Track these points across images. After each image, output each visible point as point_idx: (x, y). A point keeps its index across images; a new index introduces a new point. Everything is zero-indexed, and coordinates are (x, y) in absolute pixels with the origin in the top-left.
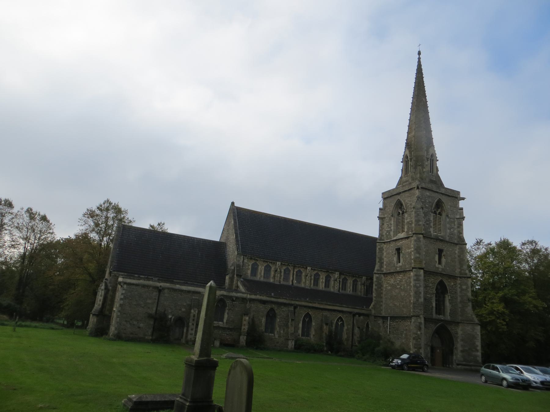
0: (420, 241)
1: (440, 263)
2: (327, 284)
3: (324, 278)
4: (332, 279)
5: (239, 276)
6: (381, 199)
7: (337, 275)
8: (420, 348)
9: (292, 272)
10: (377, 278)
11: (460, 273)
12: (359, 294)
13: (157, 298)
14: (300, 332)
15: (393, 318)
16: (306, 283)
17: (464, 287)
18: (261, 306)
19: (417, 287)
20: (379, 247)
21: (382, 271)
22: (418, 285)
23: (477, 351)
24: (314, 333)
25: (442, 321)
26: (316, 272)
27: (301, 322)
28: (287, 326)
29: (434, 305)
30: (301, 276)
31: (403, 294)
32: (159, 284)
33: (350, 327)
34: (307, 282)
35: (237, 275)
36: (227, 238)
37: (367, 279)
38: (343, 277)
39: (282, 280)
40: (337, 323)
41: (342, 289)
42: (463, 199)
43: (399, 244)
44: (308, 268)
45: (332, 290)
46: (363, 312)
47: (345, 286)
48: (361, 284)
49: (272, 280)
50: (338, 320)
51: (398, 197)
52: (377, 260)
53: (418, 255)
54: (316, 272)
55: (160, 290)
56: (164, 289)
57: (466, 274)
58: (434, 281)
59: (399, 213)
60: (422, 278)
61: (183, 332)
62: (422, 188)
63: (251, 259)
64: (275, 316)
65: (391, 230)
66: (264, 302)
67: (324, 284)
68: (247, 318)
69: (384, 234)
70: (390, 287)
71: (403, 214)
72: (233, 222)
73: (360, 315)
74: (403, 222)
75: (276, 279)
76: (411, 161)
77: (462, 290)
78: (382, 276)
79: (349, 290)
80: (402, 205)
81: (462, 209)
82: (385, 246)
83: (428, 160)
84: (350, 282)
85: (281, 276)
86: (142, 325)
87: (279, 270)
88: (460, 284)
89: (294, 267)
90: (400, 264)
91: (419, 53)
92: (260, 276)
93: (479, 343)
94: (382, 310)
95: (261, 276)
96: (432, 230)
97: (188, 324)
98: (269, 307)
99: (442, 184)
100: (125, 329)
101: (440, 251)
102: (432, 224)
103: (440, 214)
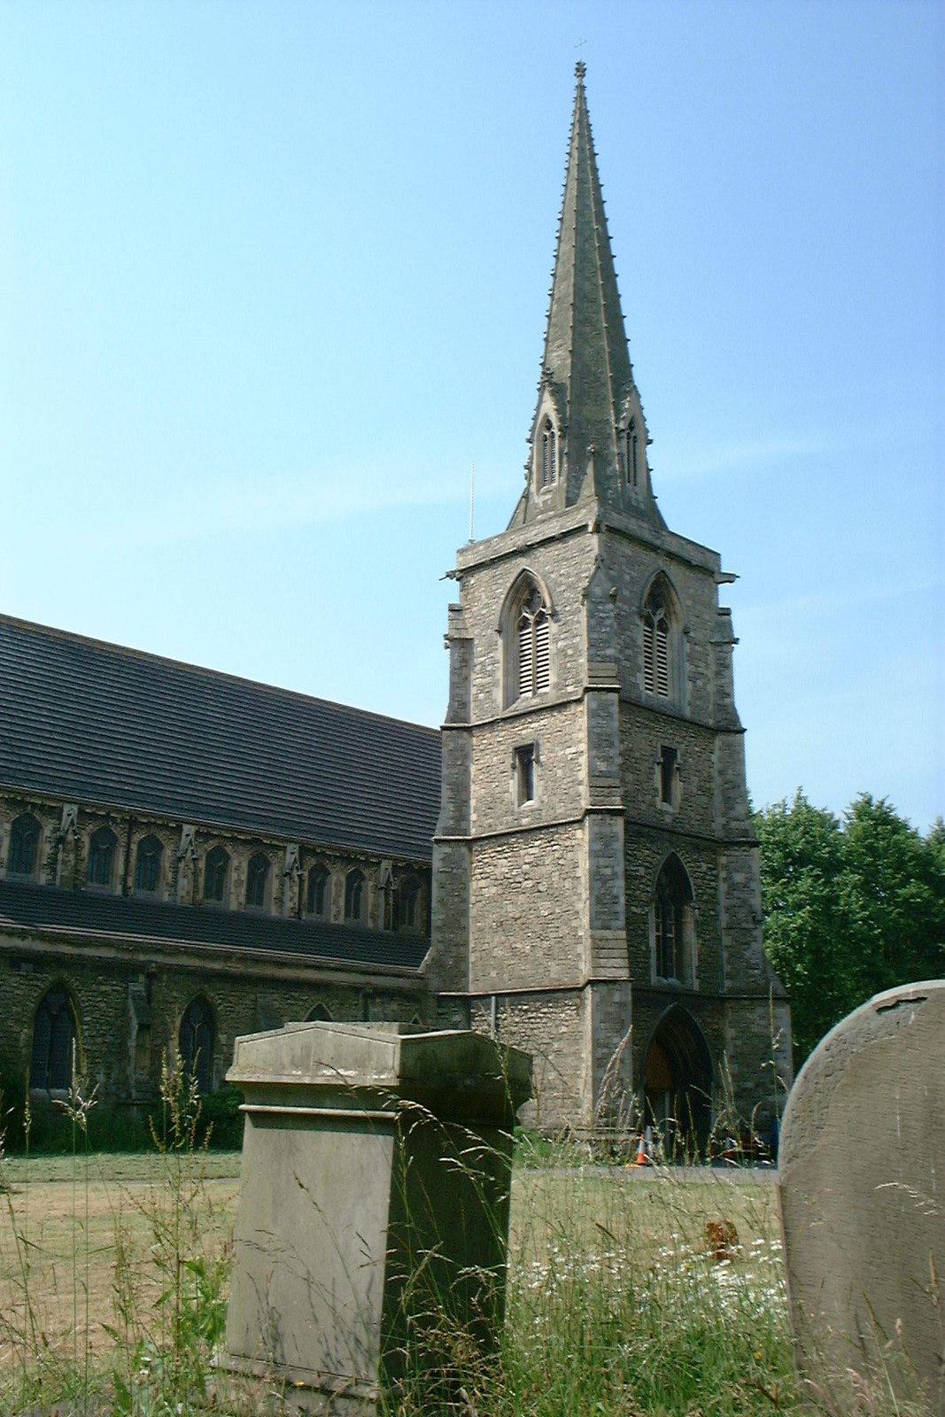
1: (667, 797)
2: (353, 906)
3: (245, 865)
4: (275, 870)
9: (123, 840)
12: (370, 924)
17: (739, 878)
20: (451, 746)
22: (608, 871)
28: (121, 1052)
29: (652, 942)
30: (156, 860)
31: (544, 908)
42: (731, 578)
43: (526, 732)
45: (274, 912)
47: (321, 894)
48: (377, 888)
51: (523, 563)
52: (446, 793)
54: (212, 844)
58: (653, 856)
60: (619, 845)
67: (243, 890)
79: (334, 910)
80: (534, 591)
81: (727, 612)
84: (337, 879)
91: (581, 70)
96: (640, 679)
99: (663, 526)
101: (669, 754)
102: (641, 660)
103: (663, 627)
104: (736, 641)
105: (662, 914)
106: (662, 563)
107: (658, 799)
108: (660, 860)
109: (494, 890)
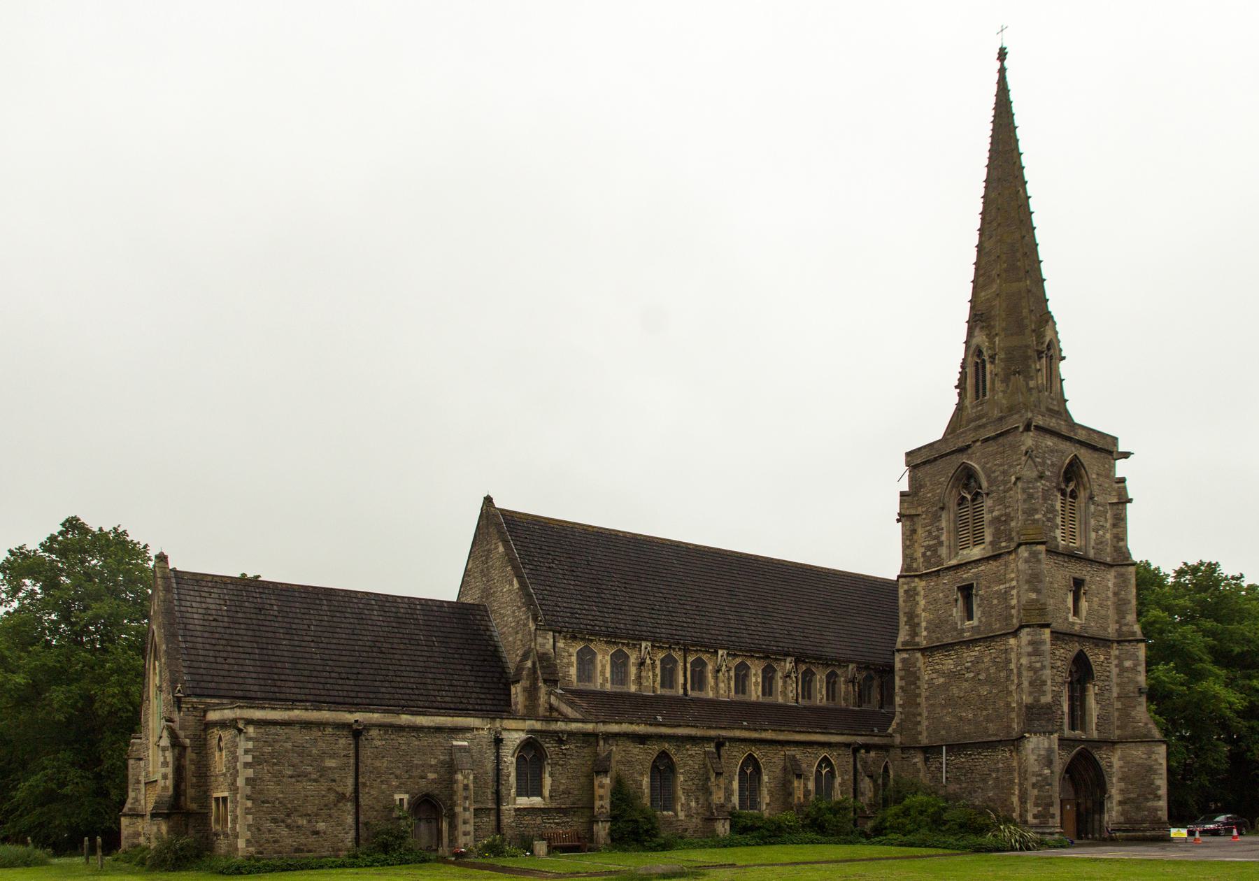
0: (1039, 561)
1: (1076, 613)
2: (768, 688)
3: (760, 672)
5: (552, 681)
6: (902, 468)
7: (789, 665)
8: (1051, 804)
9: (681, 664)
10: (903, 660)
11: (1119, 631)
12: (843, 704)
13: (352, 753)
14: (735, 799)
15: (955, 748)
16: (719, 687)
17: (1128, 664)
18: (635, 750)
19: (1036, 671)
20: (906, 587)
21: (918, 644)
22: (1038, 665)
23: (1159, 798)
24: (767, 800)
25: (1081, 741)
26: (739, 660)
27: (737, 777)
29: (1066, 708)
32: (349, 717)
33: (849, 777)
34: (722, 685)
35: (545, 681)
36: (487, 592)
37: (859, 669)
38: (803, 667)
39: (658, 685)
40: (818, 772)
41: (803, 697)
42: (1126, 455)
43: (967, 575)
44: (720, 652)
45: (780, 700)
46: (876, 740)
47: (809, 688)
48: (847, 682)
49: (633, 688)
50: (820, 765)
52: (903, 619)
53: (1034, 596)
54: (739, 660)
55: (357, 733)
56: (368, 727)
57: (1134, 633)
58: (1068, 651)
59: (964, 498)
60: (1047, 647)
61: (440, 831)
62: (1038, 428)
63: (574, 638)
64: (672, 768)
65: (941, 544)
66: (641, 739)
67: (760, 689)
68: (607, 781)
69: (919, 554)
70: (941, 680)
71: (973, 500)
72: (501, 549)
73: (868, 748)
74: (978, 519)
75: (645, 683)
76: (992, 363)
77: (1122, 670)
78: (919, 655)
79: (819, 696)
81: (1123, 480)
82: (923, 583)
83: (1040, 358)
84: (820, 677)
85: (655, 675)
86: (321, 826)
87: (648, 661)
88: (1117, 657)
89: (686, 651)
90: (975, 622)
91: (1002, 55)
92: (603, 678)
93: (1162, 783)
94: (920, 733)
95: (605, 680)
96: (1058, 533)
97: (451, 809)
98: (655, 749)
100: (275, 842)
101: (1078, 584)
102: (1059, 520)
103: (1073, 495)
104: (1130, 501)
105: (1072, 690)
106: (1070, 450)
107: (1070, 615)
108: (1071, 655)
109: (941, 680)
